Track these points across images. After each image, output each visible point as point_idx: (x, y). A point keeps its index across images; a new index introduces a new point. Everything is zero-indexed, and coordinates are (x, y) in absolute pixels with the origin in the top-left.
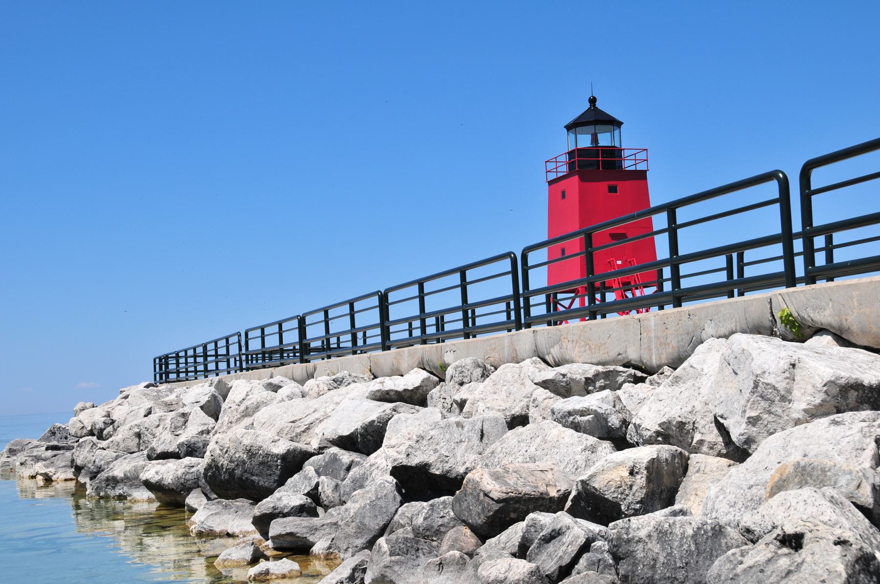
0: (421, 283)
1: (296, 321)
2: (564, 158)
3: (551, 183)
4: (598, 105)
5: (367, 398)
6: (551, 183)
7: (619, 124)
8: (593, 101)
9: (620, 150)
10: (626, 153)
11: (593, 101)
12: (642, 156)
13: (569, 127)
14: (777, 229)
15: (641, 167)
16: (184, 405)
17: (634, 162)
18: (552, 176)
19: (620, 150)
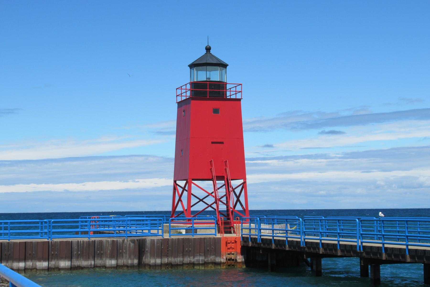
0: (140, 264)
1: (198, 233)
2: (189, 87)
3: (179, 103)
4: (211, 51)
5: (228, 65)
6: (179, 103)
7: (225, 66)
8: (208, 49)
9: (226, 84)
10: (228, 87)
11: (208, 49)
12: (239, 89)
13: (192, 66)
14: (235, 190)
15: (238, 96)
16: (150, 258)
17: (235, 93)
18: (179, 99)
19: (226, 84)
